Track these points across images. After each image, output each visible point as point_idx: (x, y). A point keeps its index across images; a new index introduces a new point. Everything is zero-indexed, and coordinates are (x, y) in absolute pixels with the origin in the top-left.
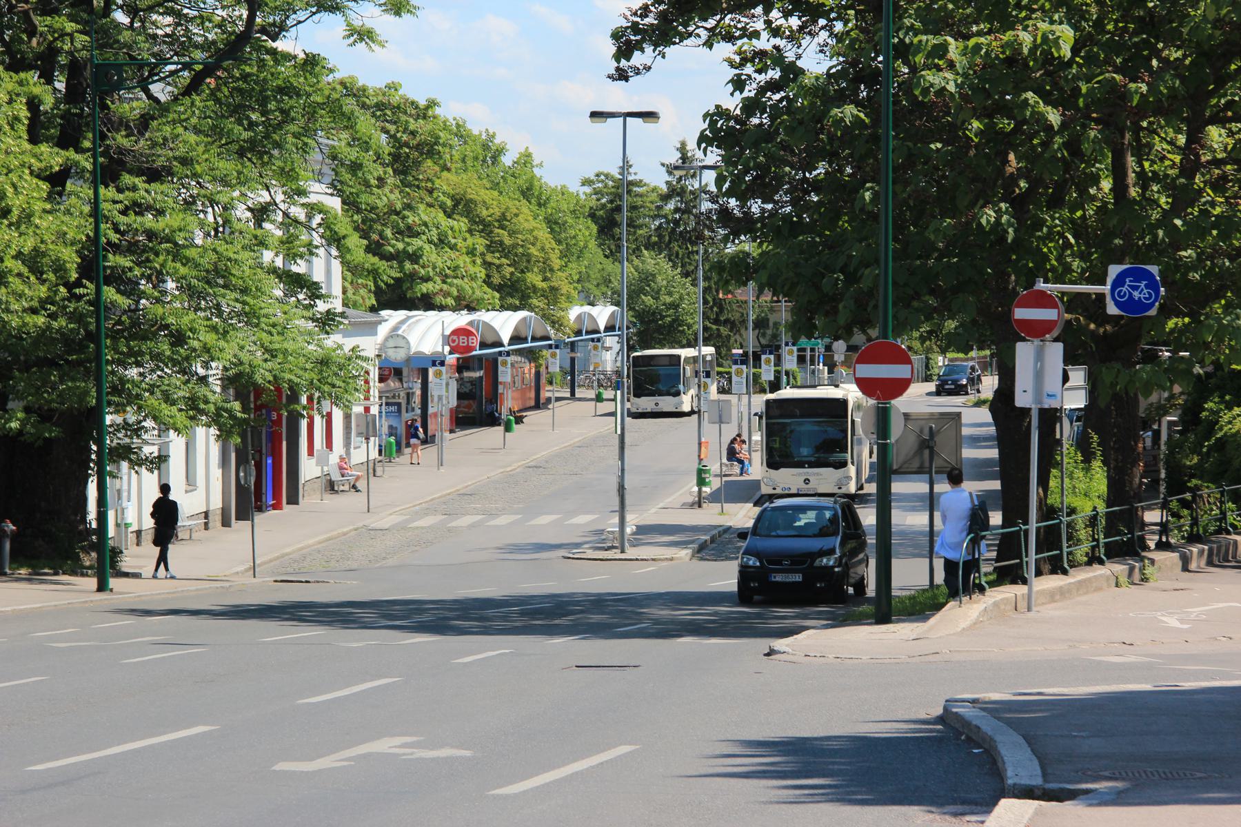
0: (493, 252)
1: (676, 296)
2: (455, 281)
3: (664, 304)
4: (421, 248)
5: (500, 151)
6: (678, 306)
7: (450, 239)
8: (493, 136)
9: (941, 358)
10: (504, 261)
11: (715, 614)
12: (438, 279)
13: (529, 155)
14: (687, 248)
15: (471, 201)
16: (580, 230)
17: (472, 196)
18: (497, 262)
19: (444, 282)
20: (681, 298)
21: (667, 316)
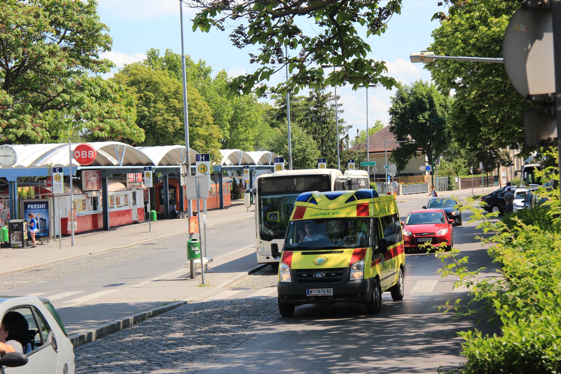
0: (169, 113)
1: (304, 145)
2: (109, 120)
3: (297, 150)
4: (82, 98)
5: (208, 71)
6: (305, 150)
7: (112, 95)
8: (204, 63)
9: (456, 178)
10: (176, 118)
11: (235, 363)
12: (96, 119)
13: (224, 73)
14: (321, 126)
15: (156, 83)
16: (252, 112)
17: (156, 80)
18: (171, 119)
19: (102, 121)
20: (307, 146)
21: (299, 156)
